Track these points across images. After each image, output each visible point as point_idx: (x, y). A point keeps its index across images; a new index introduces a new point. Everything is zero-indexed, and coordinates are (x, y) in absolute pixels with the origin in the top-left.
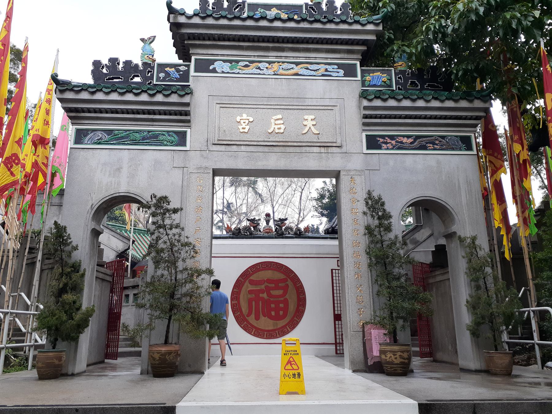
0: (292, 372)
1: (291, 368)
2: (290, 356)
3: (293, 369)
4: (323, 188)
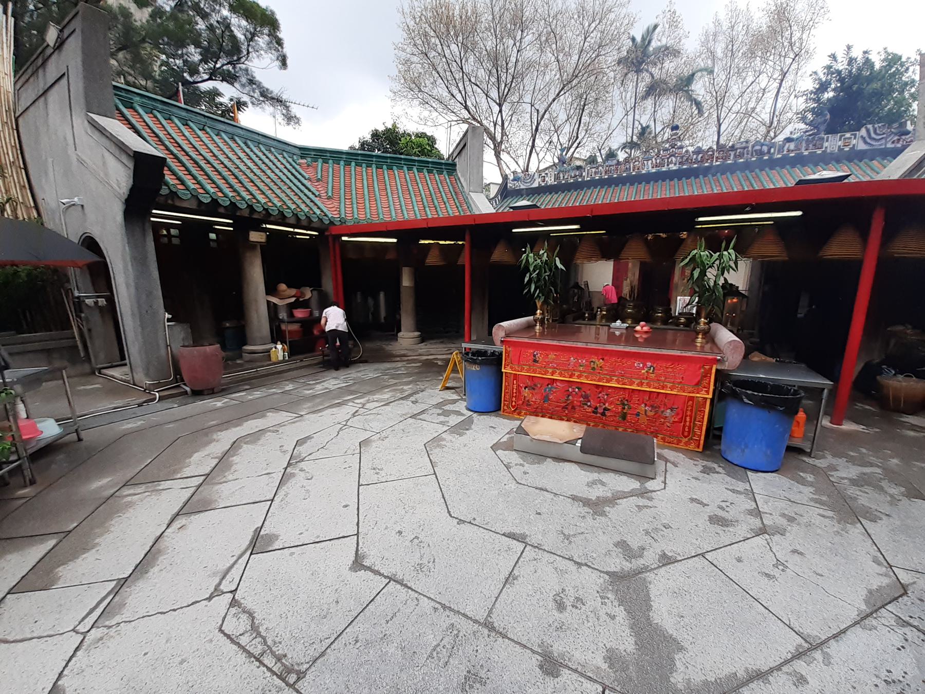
4: (829, 67)
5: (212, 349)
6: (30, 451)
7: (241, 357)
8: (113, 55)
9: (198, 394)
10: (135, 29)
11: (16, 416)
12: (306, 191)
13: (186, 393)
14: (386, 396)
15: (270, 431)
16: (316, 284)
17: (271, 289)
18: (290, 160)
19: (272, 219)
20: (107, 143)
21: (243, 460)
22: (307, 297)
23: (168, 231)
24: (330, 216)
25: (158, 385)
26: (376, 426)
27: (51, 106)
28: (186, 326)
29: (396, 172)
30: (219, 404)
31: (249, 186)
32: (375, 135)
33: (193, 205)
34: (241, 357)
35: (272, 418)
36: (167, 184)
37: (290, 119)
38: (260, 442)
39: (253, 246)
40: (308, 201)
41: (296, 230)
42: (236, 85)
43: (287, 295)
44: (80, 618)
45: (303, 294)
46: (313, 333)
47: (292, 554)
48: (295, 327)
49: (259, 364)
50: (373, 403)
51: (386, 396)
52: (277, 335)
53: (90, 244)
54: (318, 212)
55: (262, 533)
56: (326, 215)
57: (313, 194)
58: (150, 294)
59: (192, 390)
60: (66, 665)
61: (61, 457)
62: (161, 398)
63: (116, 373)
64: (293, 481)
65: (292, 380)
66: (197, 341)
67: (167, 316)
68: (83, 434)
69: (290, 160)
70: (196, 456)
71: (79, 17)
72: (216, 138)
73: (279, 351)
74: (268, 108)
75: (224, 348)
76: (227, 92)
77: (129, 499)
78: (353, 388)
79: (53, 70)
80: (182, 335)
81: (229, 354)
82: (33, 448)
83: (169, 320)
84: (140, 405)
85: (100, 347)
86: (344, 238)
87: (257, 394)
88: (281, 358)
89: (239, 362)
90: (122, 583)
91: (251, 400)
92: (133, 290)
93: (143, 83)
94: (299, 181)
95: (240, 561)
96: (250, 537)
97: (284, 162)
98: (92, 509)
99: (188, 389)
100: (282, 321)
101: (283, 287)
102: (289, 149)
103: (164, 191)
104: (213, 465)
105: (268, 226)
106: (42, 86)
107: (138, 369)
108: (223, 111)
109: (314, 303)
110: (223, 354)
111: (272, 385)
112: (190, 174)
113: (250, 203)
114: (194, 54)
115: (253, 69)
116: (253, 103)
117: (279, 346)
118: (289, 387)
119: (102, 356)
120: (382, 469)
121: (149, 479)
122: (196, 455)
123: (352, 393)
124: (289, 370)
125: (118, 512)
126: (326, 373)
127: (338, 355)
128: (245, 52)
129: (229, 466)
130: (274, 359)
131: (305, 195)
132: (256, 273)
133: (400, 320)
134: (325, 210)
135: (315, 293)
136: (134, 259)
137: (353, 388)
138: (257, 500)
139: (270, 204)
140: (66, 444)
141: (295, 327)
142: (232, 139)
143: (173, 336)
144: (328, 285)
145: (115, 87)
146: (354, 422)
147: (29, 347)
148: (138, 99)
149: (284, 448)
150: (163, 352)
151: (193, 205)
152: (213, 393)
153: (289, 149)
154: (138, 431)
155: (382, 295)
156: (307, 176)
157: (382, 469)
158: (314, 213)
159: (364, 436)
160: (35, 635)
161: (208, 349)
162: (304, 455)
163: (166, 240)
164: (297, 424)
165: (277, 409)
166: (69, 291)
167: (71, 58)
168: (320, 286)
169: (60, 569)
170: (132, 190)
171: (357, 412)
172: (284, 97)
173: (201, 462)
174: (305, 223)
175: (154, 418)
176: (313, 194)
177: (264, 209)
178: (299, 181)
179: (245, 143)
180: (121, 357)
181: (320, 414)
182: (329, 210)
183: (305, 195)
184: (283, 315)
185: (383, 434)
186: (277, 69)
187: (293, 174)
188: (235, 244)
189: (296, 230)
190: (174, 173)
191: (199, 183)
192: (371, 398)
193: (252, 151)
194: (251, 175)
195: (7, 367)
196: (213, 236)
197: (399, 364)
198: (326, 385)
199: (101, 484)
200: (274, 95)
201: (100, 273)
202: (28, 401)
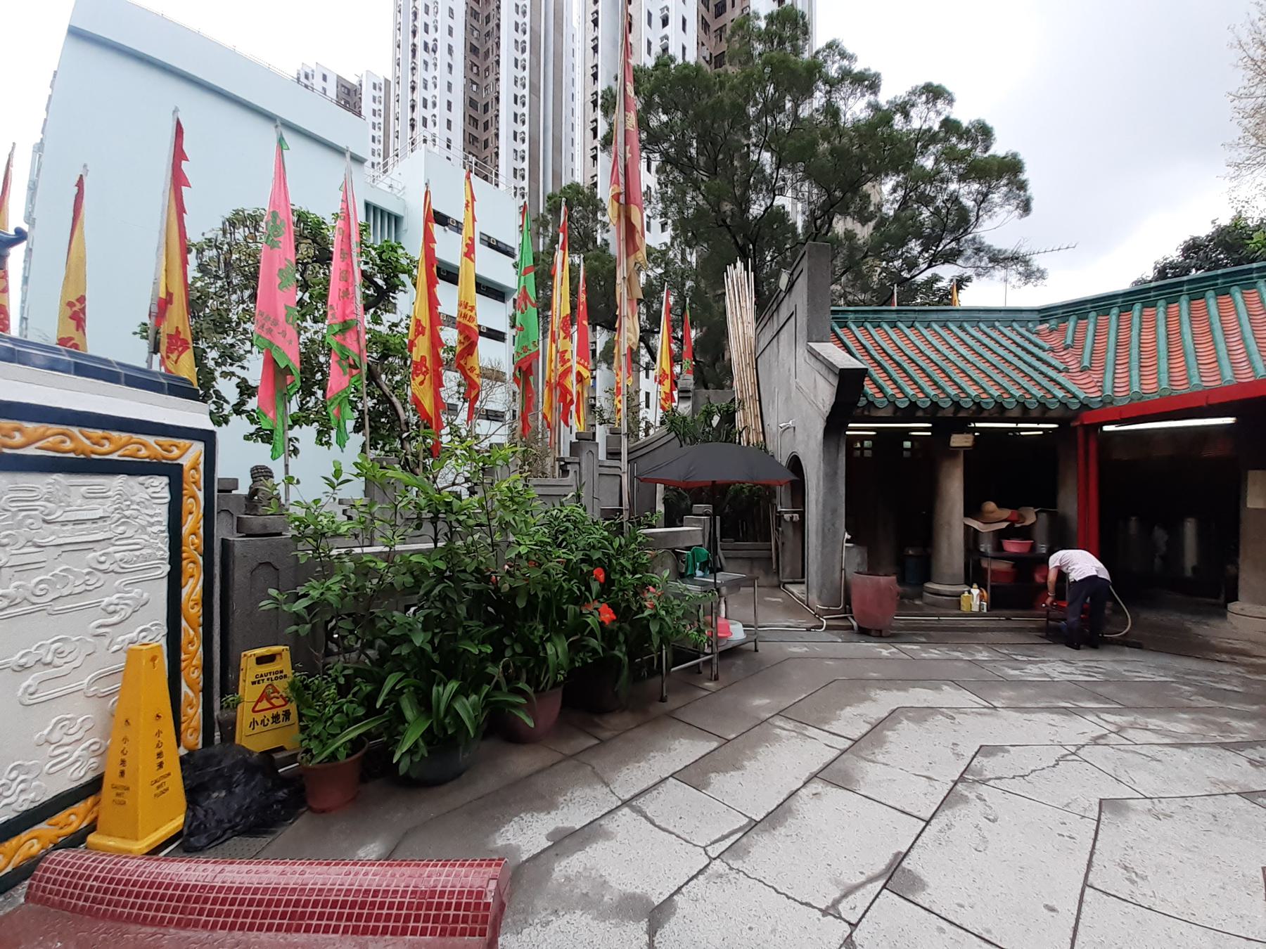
0: (269, 714)
1: (850, 743)
2: (266, 683)
3: (274, 707)
5: (887, 581)
6: (721, 649)
7: (920, 597)
8: (836, 281)
9: (865, 632)
10: (859, 249)
11: (718, 614)
12: (1044, 368)
13: (852, 628)
14: (1181, 728)
15: (942, 714)
16: (1046, 501)
17: (972, 509)
18: (1023, 331)
19: (985, 414)
20: (818, 365)
21: (902, 736)
22: (1028, 523)
23: (862, 444)
24: (1082, 396)
25: (828, 612)
26: (1146, 782)
27: (781, 344)
28: (864, 550)
29: (1238, 296)
30: (885, 653)
31: (958, 378)
32: (1193, 248)
33: (888, 413)
34: (920, 597)
35: (949, 696)
36: (865, 395)
37: (1031, 275)
38: (927, 725)
39: (954, 452)
40: (1045, 382)
41: (1020, 425)
42: (960, 262)
43: (997, 516)
44: (713, 839)
45: (1022, 518)
46: (1033, 579)
47: (941, 930)
48: (1003, 566)
49: (943, 611)
50: (1148, 732)
51: (1181, 728)
52: (974, 575)
53: (795, 464)
54: (1060, 394)
55: (904, 864)
56: (1075, 397)
57: (1055, 368)
58: (834, 511)
59: (859, 627)
60: (687, 883)
61: (739, 662)
62: (829, 628)
63: (795, 589)
64: (961, 810)
65: (990, 646)
66: (872, 569)
67: (847, 536)
68: (759, 644)
69: (1023, 331)
70: (849, 711)
71: (806, 257)
72: (925, 332)
73: (974, 598)
74: (999, 273)
75: (901, 581)
76: (947, 273)
77: (778, 731)
78: (1100, 690)
79: (784, 312)
80: (858, 560)
81: (908, 589)
82: (724, 646)
83: (848, 541)
84: (808, 630)
85: (787, 559)
86: (1106, 428)
87: (934, 653)
88: (975, 609)
89: (917, 602)
90: (753, 825)
91: (924, 659)
92: (820, 506)
93: (862, 297)
94: (1033, 355)
95: (869, 886)
96: (888, 861)
97: (1013, 336)
98: (750, 726)
99: (855, 624)
100: (984, 555)
101: (991, 506)
102: (1019, 316)
103: (863, 402)
104: (864, 731)
105: (978, 425)
106: (776, 328)
107: (809, 592)
108: (941, 297)
109: (1041, 533)
110: (899, 589)
111: (957, 646)
112: (891, 378)
113: (956, 399)
114: (915, 246)
115: (982, 234)
116: (978, 275)
117: (975, 591)
118: (983, 655)
119: (788, 570)
120: (1144, 878)
121: (808, 716)
122: (848, 709)
123: (1096, 697)
124: (986, 630)
125: (767, 741)
126: (1045, 649)
127: (1082, 623)
128: (973, 219)
129: (881, 742)
130: (965, 608)
131: (1041, 373)
132: (954, 488)
133: (1236, 578)
134: (1074, 389)
135: (1043, 516)
136: (826, 475)
137: (1100, 690)
138: (907, 810)
139: (984, 396)
140: (748, 651)
141: (1003, 566)
142: (945, 327)
143: (850, 558)
144: (1069, 503)
145: (833, 312)
146: (1095, 754)
147: (740, 554)
148: (851, 316)
149: (959, 749)
150: (837, 575)
151: (1016, 413)
152: (881, 636)
153: (1019, 316)
154: (801, 657)
155: (1190, 527)
156: (1047, 346)
157: (1144, 878)
158: (1054, 397)
159: (1114, 791)
160: (675, 831)
161: (883, 580)
162: (988, 775)
163: (858, 452)
164: (986, 719)
165: (958, 684)
166: (774, 506)
167: (799, 299)
168: (1055, 505)
169: (713, 775)
170: (834, 407)
171: (1103, 737)
172: (1023, 251)
173: (852, 720)
174: (1034, 414)
175: (818, 649)
176: (1055, 368)
177: (975, 403)
178: (1033, 355)
179: (961, 327)
180: (800, 576)
181: (1027, 716)
182: (1084, 389)
183: (1041, 373)
184: (986, 547)
185: (1162, 806)
186: (1016, 220)
187: (1024, 349)
188: (933, 453)
189: (1020, 425)
190: (874, 382)
191: (899, 387)
192: (1141, 720)
193: (968, 333)
194: (962, 364)
195: (721, 570)
196: (907, 444)
197: (1226, 670)
198: (1046, 668)
199: (760, 703)
200: (1008, 254)
201: (798, 489)
202: (729, 602)
